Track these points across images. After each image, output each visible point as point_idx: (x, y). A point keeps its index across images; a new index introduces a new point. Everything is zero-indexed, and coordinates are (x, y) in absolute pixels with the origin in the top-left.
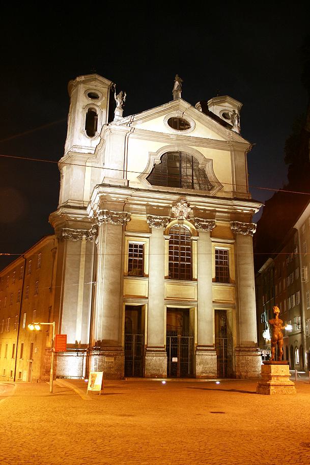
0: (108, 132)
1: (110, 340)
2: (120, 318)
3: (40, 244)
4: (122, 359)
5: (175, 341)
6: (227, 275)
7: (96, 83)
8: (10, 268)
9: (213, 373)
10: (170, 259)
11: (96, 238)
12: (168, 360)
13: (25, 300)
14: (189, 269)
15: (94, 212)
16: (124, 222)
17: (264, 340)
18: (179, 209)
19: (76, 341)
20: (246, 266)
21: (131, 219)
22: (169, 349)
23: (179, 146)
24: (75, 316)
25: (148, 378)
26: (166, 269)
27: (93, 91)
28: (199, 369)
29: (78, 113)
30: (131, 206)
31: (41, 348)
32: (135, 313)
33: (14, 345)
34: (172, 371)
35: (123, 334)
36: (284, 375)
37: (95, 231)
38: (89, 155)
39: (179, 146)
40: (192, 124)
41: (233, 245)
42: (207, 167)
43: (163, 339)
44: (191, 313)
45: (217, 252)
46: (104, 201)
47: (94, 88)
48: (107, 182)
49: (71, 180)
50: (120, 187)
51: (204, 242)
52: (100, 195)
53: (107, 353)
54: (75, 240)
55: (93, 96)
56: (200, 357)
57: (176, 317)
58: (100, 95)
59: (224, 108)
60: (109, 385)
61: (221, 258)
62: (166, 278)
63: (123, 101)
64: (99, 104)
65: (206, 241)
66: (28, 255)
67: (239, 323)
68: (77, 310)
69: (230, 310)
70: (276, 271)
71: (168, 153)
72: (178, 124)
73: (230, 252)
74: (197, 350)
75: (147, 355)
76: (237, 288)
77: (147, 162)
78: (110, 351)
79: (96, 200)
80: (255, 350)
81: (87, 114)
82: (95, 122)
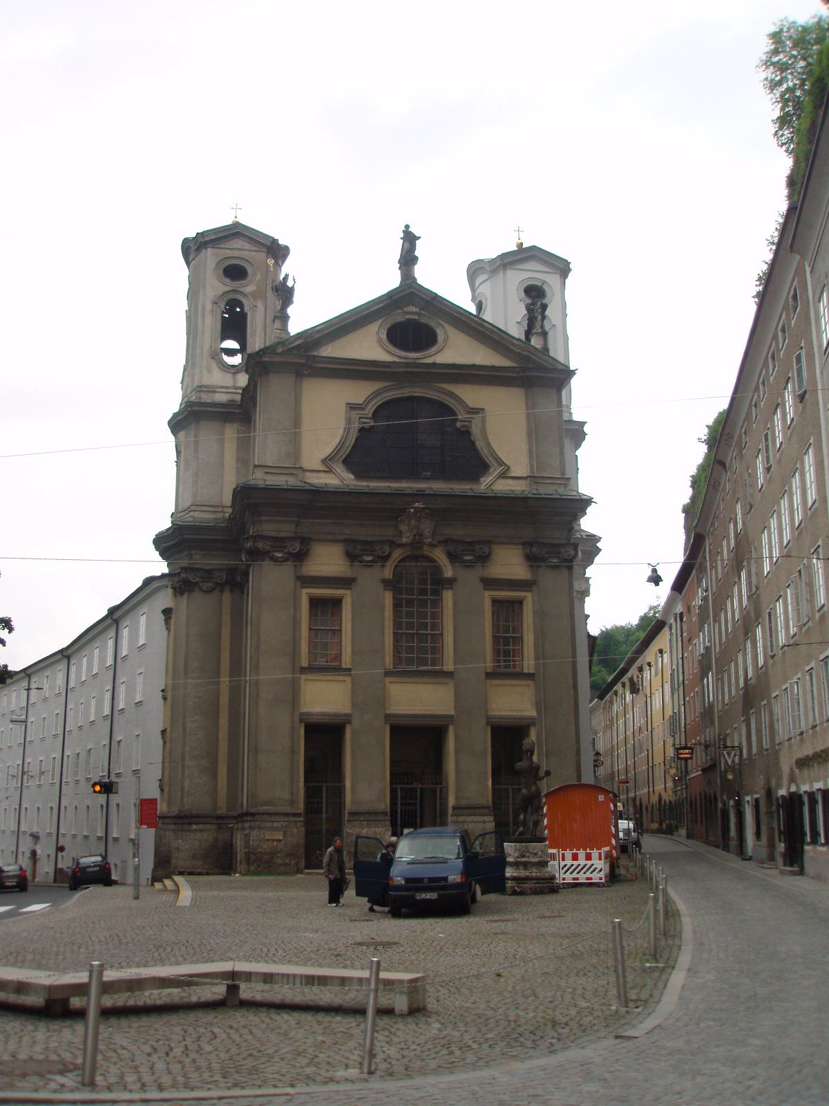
22: (396, 811)
35: (302, 784)
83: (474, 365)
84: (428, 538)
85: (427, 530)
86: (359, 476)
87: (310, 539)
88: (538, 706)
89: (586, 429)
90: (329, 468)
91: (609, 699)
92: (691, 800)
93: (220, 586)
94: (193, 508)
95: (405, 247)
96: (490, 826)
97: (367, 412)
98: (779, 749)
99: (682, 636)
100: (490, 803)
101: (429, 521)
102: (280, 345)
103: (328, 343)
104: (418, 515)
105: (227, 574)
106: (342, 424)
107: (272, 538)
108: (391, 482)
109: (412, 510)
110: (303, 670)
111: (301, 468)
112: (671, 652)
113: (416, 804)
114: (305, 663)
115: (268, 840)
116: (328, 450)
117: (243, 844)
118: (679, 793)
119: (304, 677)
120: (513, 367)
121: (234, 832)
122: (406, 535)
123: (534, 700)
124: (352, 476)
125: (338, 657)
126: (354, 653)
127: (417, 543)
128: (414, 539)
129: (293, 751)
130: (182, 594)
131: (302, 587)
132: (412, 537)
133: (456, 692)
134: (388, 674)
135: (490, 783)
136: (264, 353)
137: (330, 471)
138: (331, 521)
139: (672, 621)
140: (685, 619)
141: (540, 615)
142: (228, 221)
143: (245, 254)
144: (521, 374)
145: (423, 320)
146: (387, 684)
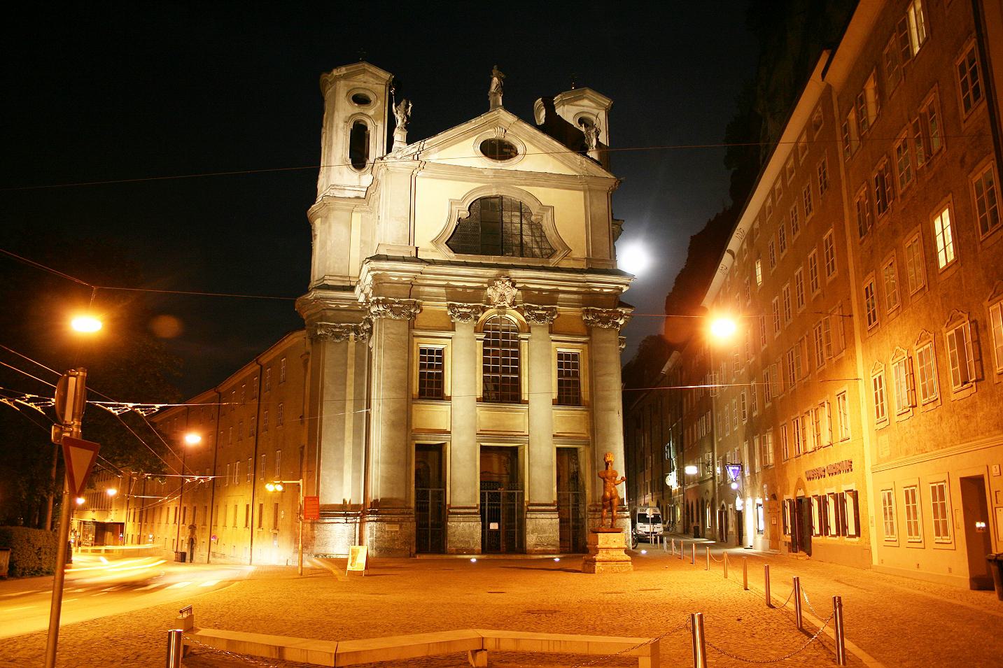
0: (383, 170)
1: (391, 499)
2: (408, 464)
3: (283, 343)
4: (411, 527)
5: (495, 497)
6: (577, 394)
7: (366, 77)
8: (235, 379)
9: (553, 545)
10: (486, 370)
11: (370, 337)
12: (483, 527)
13: (263, 434)
14: (517, 384)
15: (367, 296)
16: (410, 315)
17: (669, 489)
18: (498, 290)
19: (344, 500)
20: (608, 378)
21: (421, 310)
22: (485, 509)
23: (498, 186)
24: (341, 460)
25: (452, 554)
26: (478, 386)
27: (361, 92)
28: (531, 540)
29: (337, 131)
30: (422, 289)
31: (290, 510)
32: (434, 454)
33: (248, 506)
34: (491, 544)
36: (616, 547)
37: (369, 326)
38: (355, 200)
39: (498, 186)
40: (520, 149)
41: (586, 346)
42: (545, 219)
43: (476, 495)
44: (520, 453)
45: (560, 356)
46: (378, 282)
47: (363, 85)
48: (383, 252)
49: (329, 243)
50: (404, 260)
51: (540, 343)
52: (373, 273)
53: (388, 518)
54: (338, 341)
55: (361, 100)
56: (533, 521)
57: (500, 459)
58: (372, 97)
59: (581, 109)
60: (391, 565)
61: (568, 365)
62: (478, 400)
63: (407, 116)
64: (371, 113)
65: (542, 340)
66: (265, 359)
67: (595, 469)
68: (343, 452)
69: (582, 448)
70: (684, 374)
71: (481, 199)
72: (497, 150)
73: (581, 357)
74: (529, 511)
75: (450, 519)
76: (593, 413)
77: (447, 215)
78: (393, 514)
79: (367, 279)
80: (621, 509)
81: (310, 282)
82: (367, 140)
92: (688, 506)
98: (786, 465)
135: (555, 489)
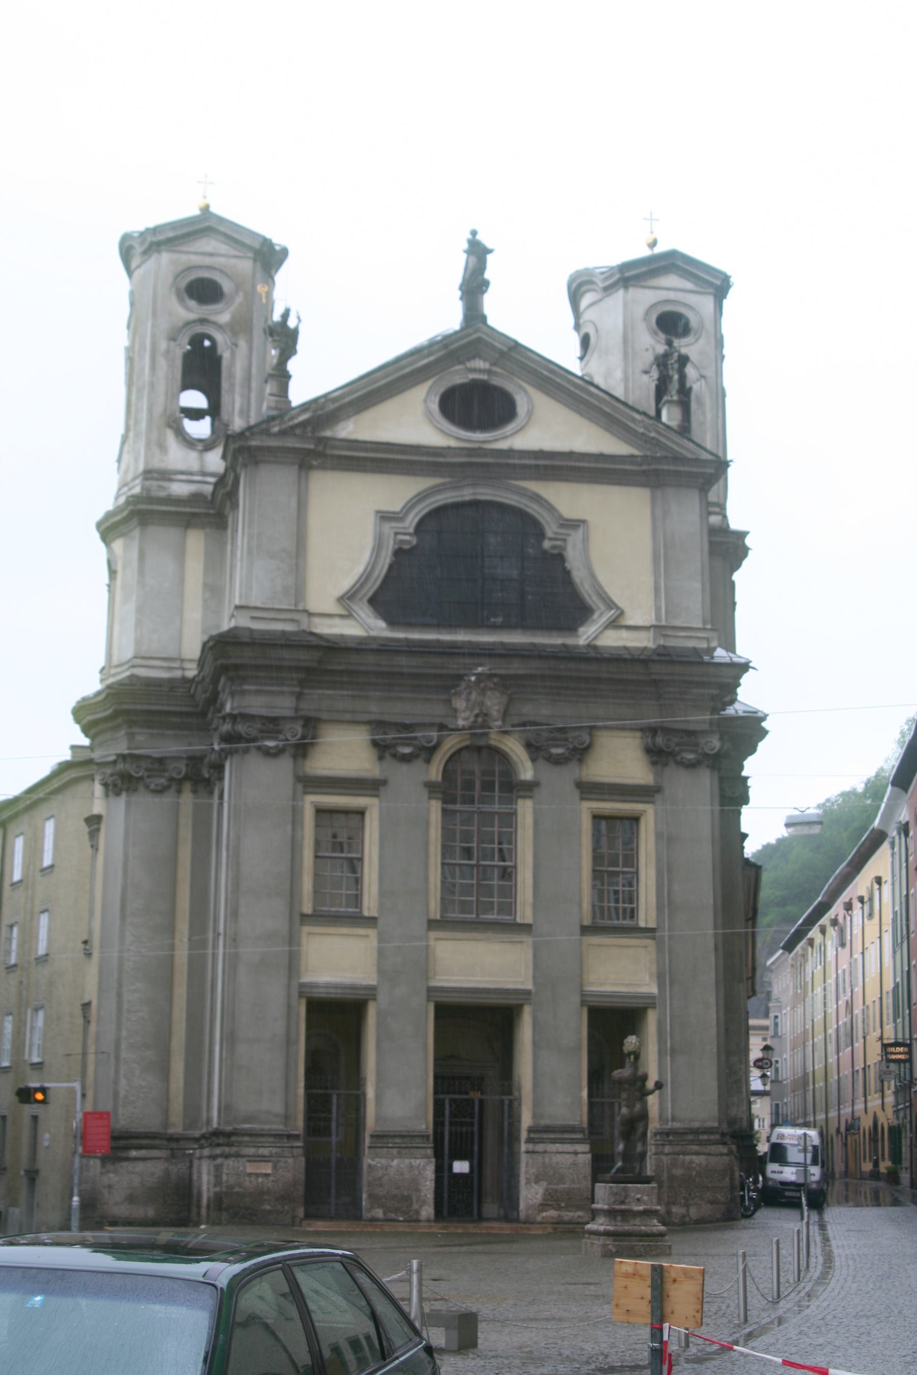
12: (439, 1170)
22: (442, 1134)
35: (301, 1091)
83: (570, 455)
84: (496, 720)
85: (496, 708)
86: (392, 623)
87: (318, 720)
88: (660, 978)
89: (748, 541)
90: (348, 611)
91: (800, 953)
93: (176, 784)
94: (139, 661)
95: (471, 265)
96: (585, 1159)
97: (407, 523)
99: (907, 861)
100: (585, 1125)
101: (498, 694)
102: (277, 422)
103: (349, 417)
104: (482, 685)
105: (187, 765)
106: (369, 542)
107: (261, 717)
108: (439, 633)
109: (473, 678)
110: (304, 918)
111: (306, 611)
112: (893, 884)
113: (472, 1124)
114: (307, 908)
115: (250, 1175)
116: (346, 583)
117: (212, 1179)
118: (901, 1114)
119: (306, 929)
120: (632, 456)
121: (196, 1162)
122: (463, 715)
123: (654, 969)
124: (382, 624)
125: (357, 900)
126: (382, 894)
127: (482, 720)
128: (475, 721)
129: (289, 1042)
130: (118, 794)
131: (306, 793)
132: (472, 719)
133: (535, 956)
134: (433, 924)
135: (585, 1093)
136: (252, 434)
137: (349, 616)
138: (350, 693)
139: (895, 833)
140: (911, 834)
141: (665, 839)
142: (192, 211)
143: (219, 261)
144: (644, 467)
145: (496, 381)
146: (432, 943)
